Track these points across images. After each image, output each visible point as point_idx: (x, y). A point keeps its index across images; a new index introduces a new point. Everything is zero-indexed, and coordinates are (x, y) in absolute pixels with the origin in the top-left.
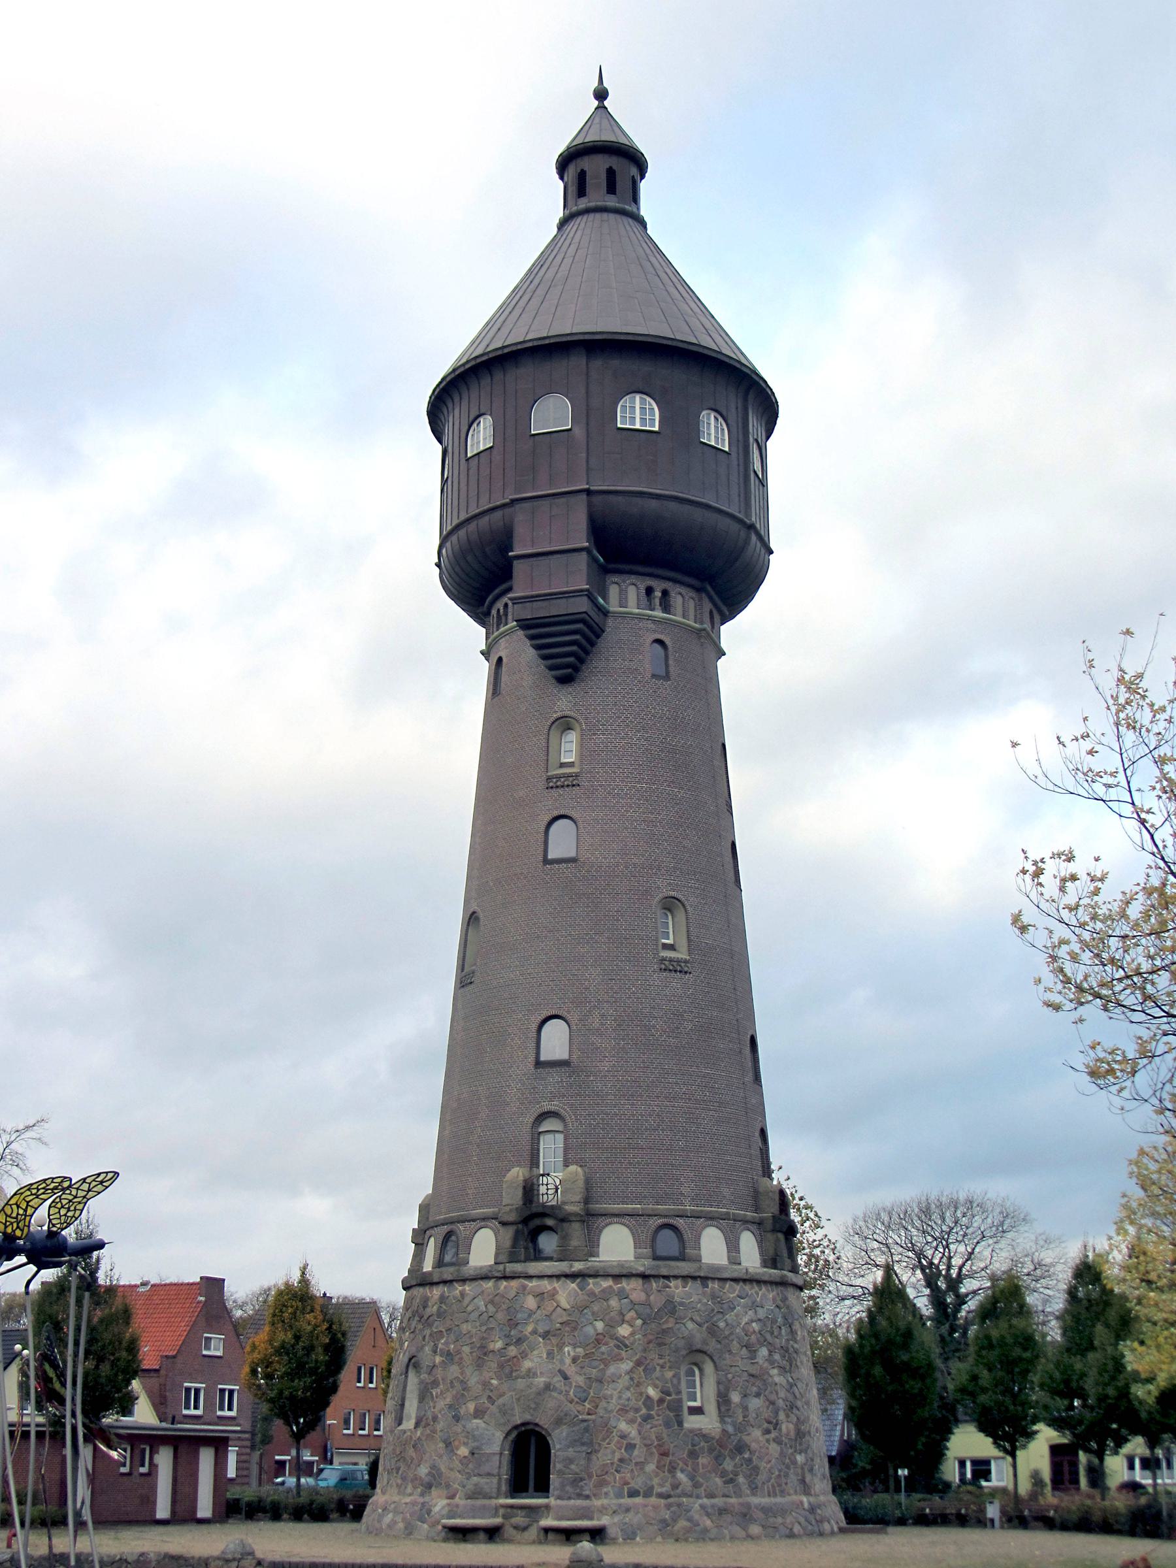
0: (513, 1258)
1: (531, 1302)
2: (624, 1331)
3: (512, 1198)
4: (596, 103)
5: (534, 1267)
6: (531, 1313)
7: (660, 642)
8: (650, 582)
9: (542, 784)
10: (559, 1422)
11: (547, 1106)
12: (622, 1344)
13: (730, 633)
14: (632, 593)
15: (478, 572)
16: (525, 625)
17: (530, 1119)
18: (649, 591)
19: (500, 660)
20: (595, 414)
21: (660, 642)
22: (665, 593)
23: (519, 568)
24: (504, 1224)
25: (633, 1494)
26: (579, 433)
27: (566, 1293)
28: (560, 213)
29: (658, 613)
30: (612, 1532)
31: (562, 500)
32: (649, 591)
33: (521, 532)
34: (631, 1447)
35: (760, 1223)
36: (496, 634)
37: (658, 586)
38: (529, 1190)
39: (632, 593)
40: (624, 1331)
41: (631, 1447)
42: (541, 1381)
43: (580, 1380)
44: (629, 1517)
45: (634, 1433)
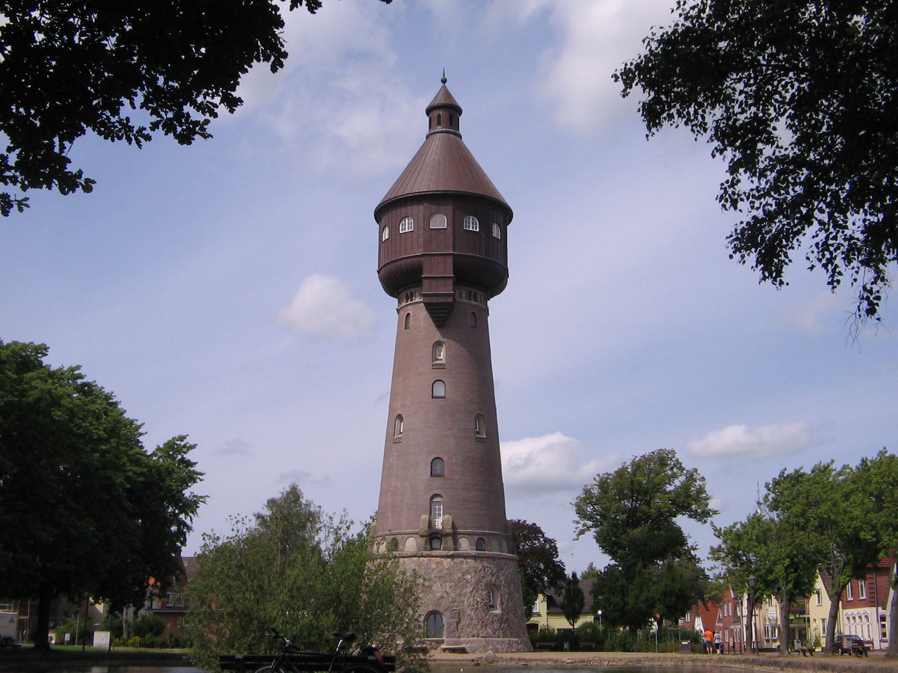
0: (425, 549)
1: (433, 566)
2: (469, 577)
3: (423, 527)
4: (442, 84)
5: (435, 553)
6: (434, 570)
7: (474, 313)
8: (471, 289)
9: (431, 366)
10: (446, 610)
11: (435, 492)
12: (467, 582)
13: (492, 303)
14: (464, 294)
15: (399, 279)
16: (428, 306)
17: (429, 497)
18: (470, 292)
19: (409, 314)
20: (456, 224)
21: (474, 313)
22: (475, 294)
23: (426, 283)
24: (421, 536)
25: (473, 636)
26: (450, 230)
27: (447, 562)
28: (426, 131)
29: (473, 302)
30: (468, 650)
31: (440, 259)
32: (470, 292)
33: (425, 268)
34: (472, 619)
35: (507, 537)
36: (404, 304)
37: (473, 291)
38: (430, 524)
39: (464, 294)
40: (469, 577)
41: (472, 619)
42: (438, 595)
43: (453, 595)
44: (473, 645)
45: (472, 614)
